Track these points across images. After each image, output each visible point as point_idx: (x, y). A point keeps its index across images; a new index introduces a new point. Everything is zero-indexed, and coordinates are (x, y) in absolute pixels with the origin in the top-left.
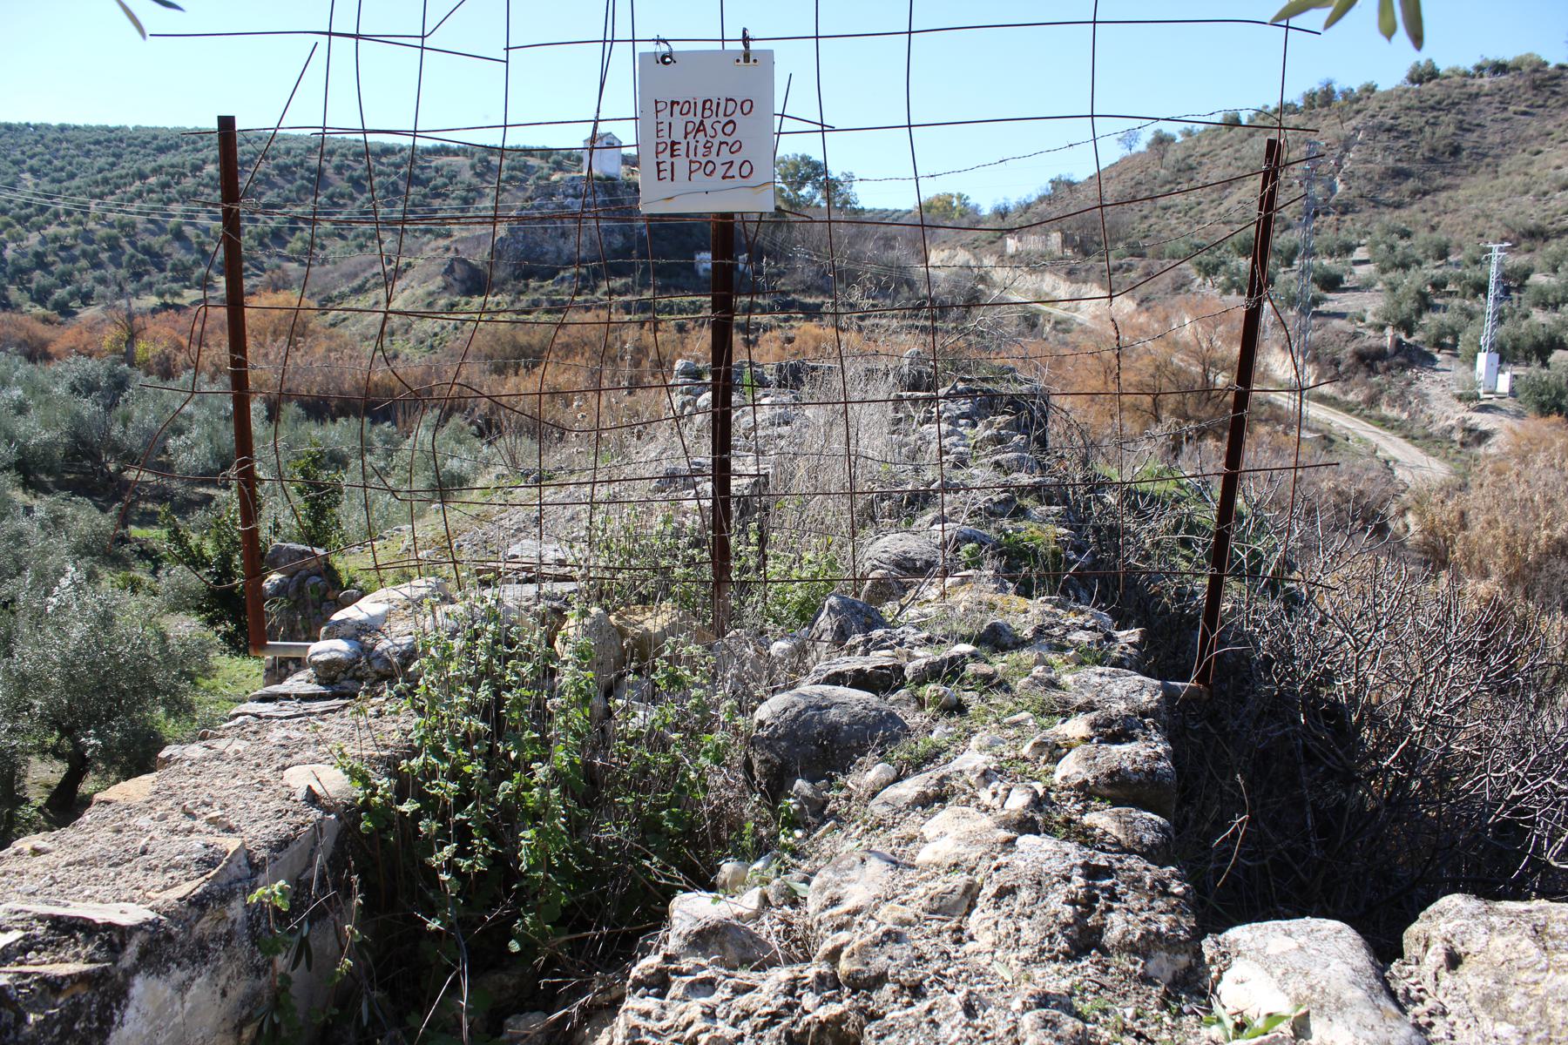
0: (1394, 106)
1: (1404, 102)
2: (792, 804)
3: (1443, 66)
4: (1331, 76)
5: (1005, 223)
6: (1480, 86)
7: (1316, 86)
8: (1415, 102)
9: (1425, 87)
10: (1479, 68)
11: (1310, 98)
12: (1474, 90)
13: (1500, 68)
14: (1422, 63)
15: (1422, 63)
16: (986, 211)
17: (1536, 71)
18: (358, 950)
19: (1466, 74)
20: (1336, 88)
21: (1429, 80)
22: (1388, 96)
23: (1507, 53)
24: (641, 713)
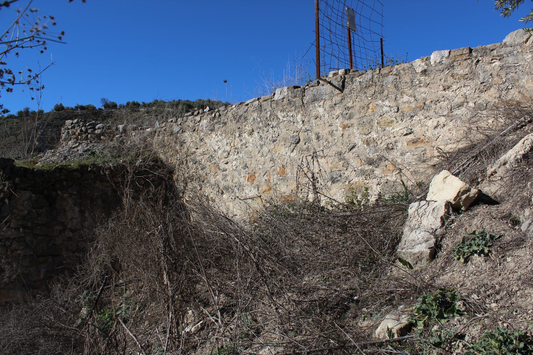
0: (50, 117)
1: (55, 116)
2: (98, 132)
3: (65, 105)
4: (28, 106)
5: (122, 107)
6: (78, 113)
7: (22, 109)
8: (58, 116)
9: (60, 112)
10: (76, 107)
11: (20, 113)
12: (76, 114)
13: (82, 108)
14: (59, 104)
15: (59, 104)
16: (97, 108)
17: (93, 109)
18: (425, 55)
19: (72, 109)
20: (30, 110)
21: (62, 110)
22: (49, 114)
23: (85, 104)
24: (37, 143)
